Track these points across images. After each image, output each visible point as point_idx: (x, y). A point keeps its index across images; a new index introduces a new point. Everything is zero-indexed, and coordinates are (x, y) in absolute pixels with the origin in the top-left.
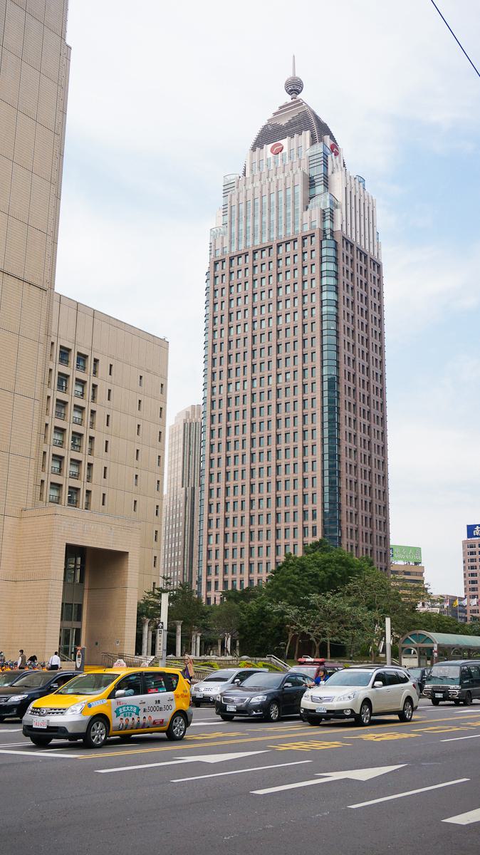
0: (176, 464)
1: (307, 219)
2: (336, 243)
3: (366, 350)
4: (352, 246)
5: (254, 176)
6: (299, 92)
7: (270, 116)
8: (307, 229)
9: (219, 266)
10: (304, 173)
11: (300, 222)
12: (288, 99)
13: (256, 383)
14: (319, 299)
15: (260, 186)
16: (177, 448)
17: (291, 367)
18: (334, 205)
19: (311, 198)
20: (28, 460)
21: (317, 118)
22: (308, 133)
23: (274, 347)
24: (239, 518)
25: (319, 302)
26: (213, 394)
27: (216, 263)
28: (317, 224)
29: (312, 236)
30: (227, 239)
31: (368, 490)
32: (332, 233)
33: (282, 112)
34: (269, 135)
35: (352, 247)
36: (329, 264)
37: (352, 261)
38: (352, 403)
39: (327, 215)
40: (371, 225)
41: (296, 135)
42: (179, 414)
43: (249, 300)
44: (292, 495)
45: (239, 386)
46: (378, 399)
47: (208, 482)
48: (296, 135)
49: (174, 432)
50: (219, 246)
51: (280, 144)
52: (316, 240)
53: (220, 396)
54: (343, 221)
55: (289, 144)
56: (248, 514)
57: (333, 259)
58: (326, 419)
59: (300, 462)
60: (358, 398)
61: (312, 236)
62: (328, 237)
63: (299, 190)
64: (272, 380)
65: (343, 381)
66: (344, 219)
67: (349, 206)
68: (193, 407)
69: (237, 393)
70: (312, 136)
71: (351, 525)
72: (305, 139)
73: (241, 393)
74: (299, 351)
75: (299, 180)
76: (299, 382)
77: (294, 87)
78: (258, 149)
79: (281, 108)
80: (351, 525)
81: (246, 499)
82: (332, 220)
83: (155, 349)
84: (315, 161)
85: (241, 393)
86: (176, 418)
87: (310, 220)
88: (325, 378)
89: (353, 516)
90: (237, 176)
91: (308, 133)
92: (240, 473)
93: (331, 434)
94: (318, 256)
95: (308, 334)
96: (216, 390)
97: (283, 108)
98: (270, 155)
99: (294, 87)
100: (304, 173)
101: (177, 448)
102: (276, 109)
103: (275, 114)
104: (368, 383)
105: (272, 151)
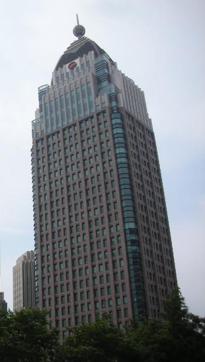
0: (19, 286)
2: (122, 115)
4: (133, 119)
5: (60, 90)
8: (100, 108)
9: (39, 144)
15: (63, 88)
16: (18, 281)
17: (98, 204)
18: (117, 91)
19: (99, 90)
21: (96, 45)
22: (93, 52)
23: (84, 192)
26: (41, 231)
27: (37, 142)
28: (107, 104)
29: (104, 112)
31: (158, 236)
32: (118, 109)
33: (73, 46)
34: (67, 59)
35: (133, 119)
36: (121, 149)
37: (139, 166)
38: (152, 273)
39: (113, 98)
41: (84, 55)
42: (19, 259)
43: (62, 153)
46: (170, 268)
49: (16, 270)
51: (74, 62)
52: (107, 114)
54: (124, 102)
55: (80, 61)
61: (104, 112)
63: (91, 85)
65: (145, 257)
66: (125, 100)
72: (91, 56)
76: (105, 214)
78: (59, 68)
79: (72, 44)
81: (71, 305)
84: (100, 66)
88: (130, 255)
89: (154, 288)
91: (93, 52)
93: (136, 273)
94: (110, 125)
95: (110, 189)
98: (68, 70)
101: (18, 281)
104: (155, 213)
105: (69, 67)
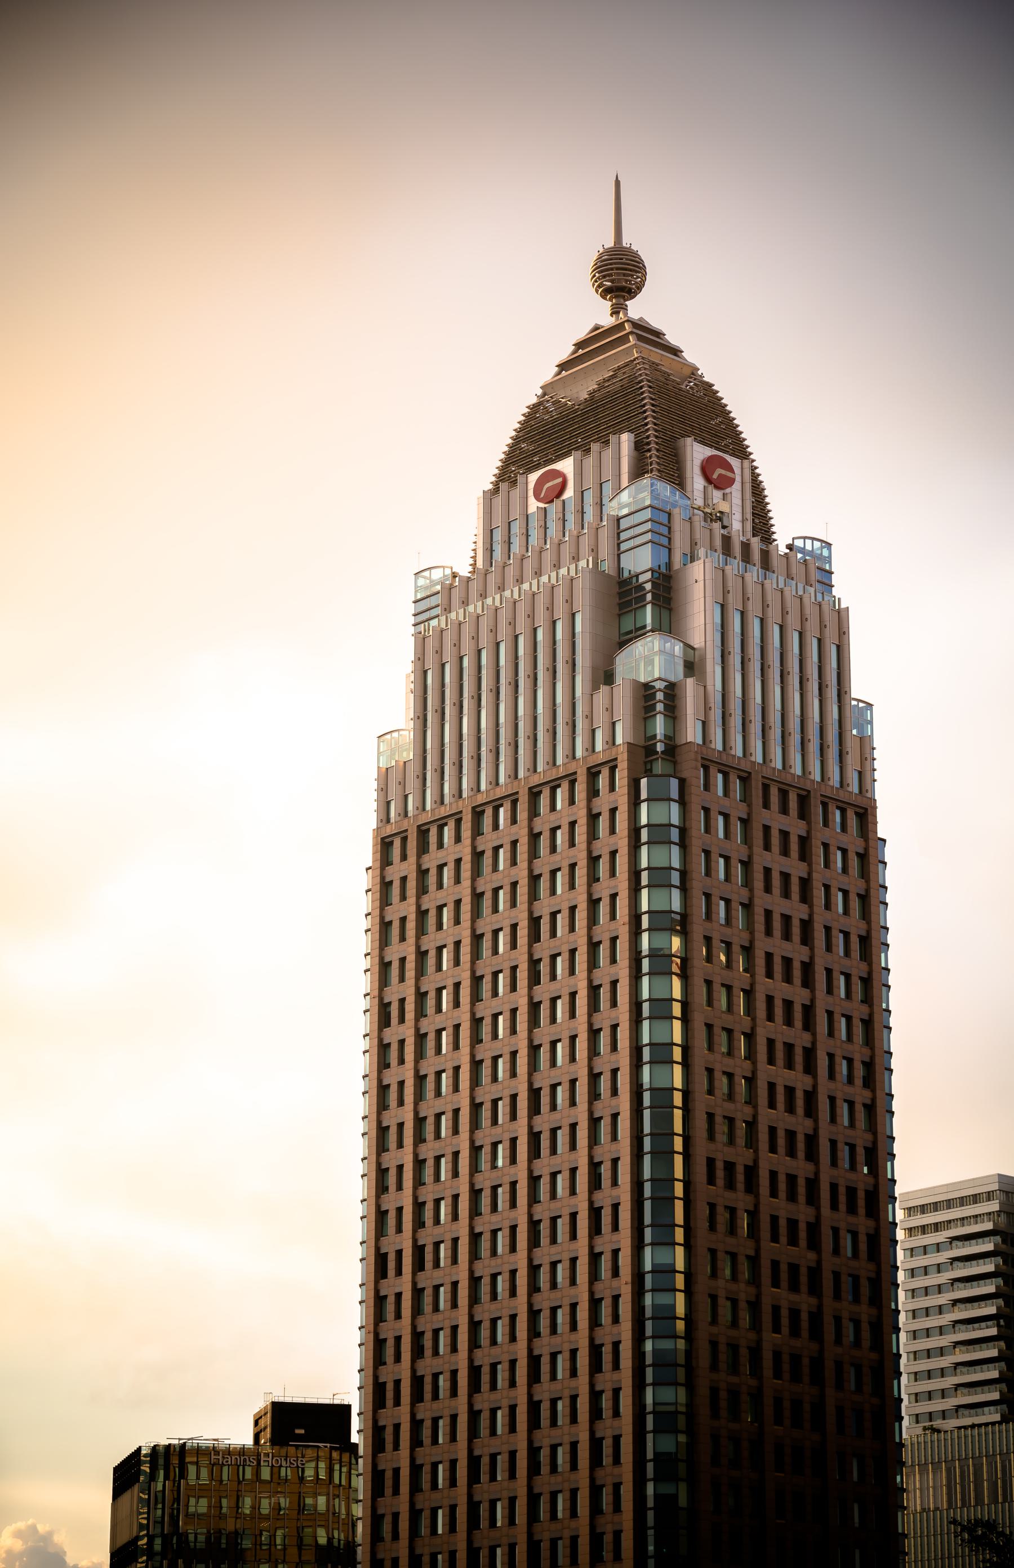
6: (631, 292)
7: (548, 373)
12: (600, 313)
32: (672, 750)
34: (545, 435)
35: (745, 779)
40: (832, 693)
41: (595, 447)
48: (595, 447)
67: (735, 660)
70: (640, 447)
71: (794, 1297)
77: (620, 274)
79: (579, 345)
80: (734, 1379)
90: (448, 572)
91: (626, 440)
97: (592, 346)
99: (620, 274)
102: (565, 352)
103: (563, 366)
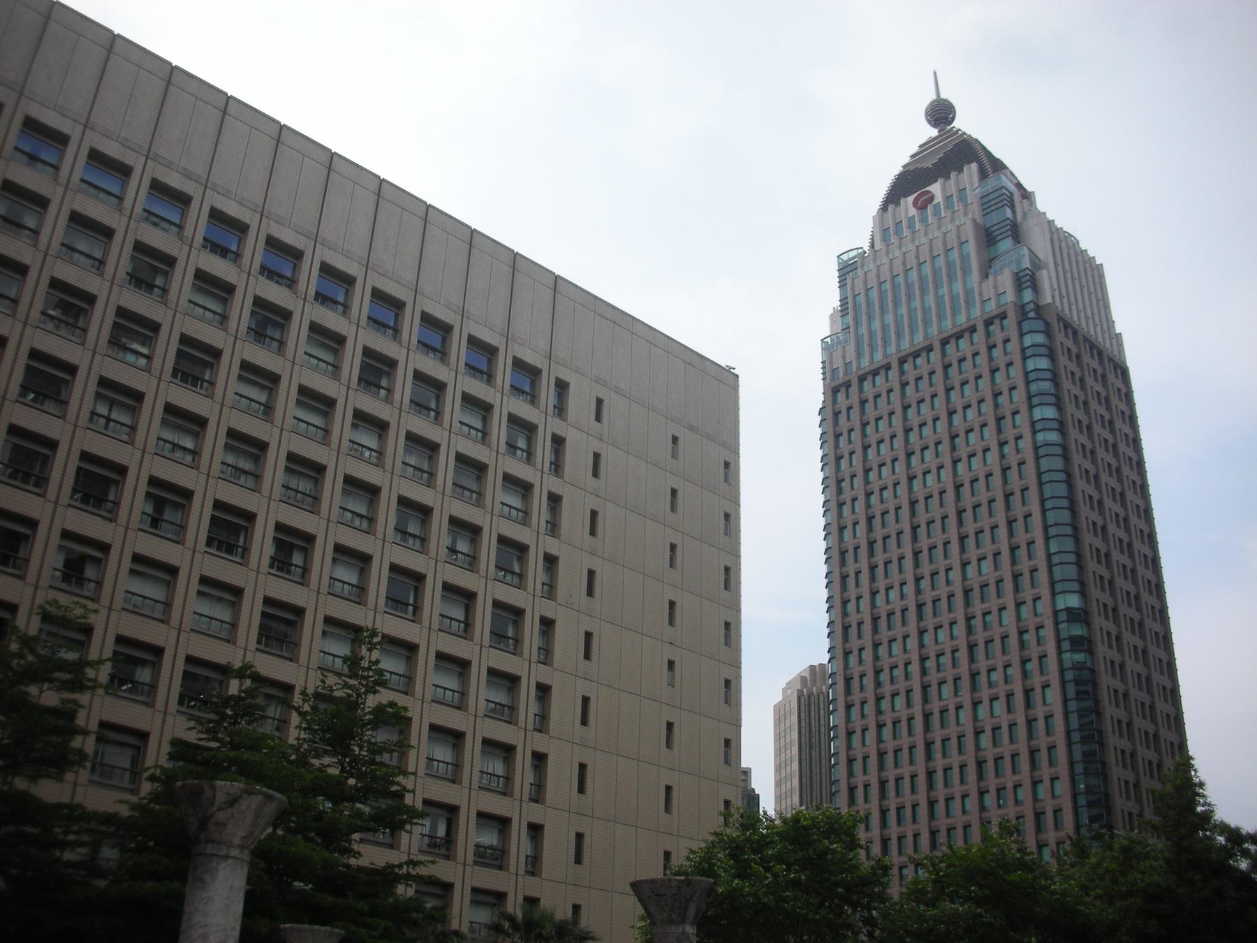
1: (988, 291)
2: (1047, 324)
3: (1137, 617)
8: (992, 307)
10: (974, 221)
11: (977, 298)
13: (925, 584)
14: (1027, 419)
18: (1037, 264)
20: (566, 814)
22: (974, 166)
24: (910, 839)
25: (1028, 424)
28: (1010, 297)
29: (1003, 316)
30: (851, 349)
32: (1038, 309)
34: (909, 183)
41: (953, 175)
43: (899, 467)
44: (1010, 786)
45: (896, 648)
47: (845, 775)
50: (838, 363)
52: (1011, 322)
53: (859, 616)
54: (1053, 290)
55: (944, 189)
56: (927, 829)
57: (1052, 400)
58: (1078, 756)
59: (1021, 720)
60: (1138, 741)
61: (1003, 316)
62: (1032, 315)
63: (971, 248)
64: (955, 575)
65: (1107, 681)
66: (1056, 287)
68: (812, 668)
69: (889, 607)
72: (970, 176)
73: (897, 606)
74: (1000, 517)
75: (969, 233)
77: (941, 113)
78: (891, 207)
82: (1035, 287)
83: (702, 397)
85: (897, 606)
86: (784, 690)
87: (1000, 289)
91: (974, 166)
92: (907, 782)
93: (1084, 720)
96: (851, 607)
98: (913, 211)
99: (941, 113)
100: (974, 221)
105: (915, 204)
